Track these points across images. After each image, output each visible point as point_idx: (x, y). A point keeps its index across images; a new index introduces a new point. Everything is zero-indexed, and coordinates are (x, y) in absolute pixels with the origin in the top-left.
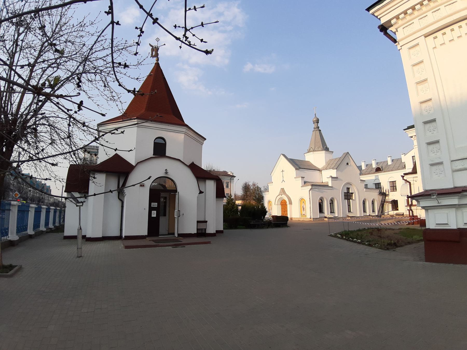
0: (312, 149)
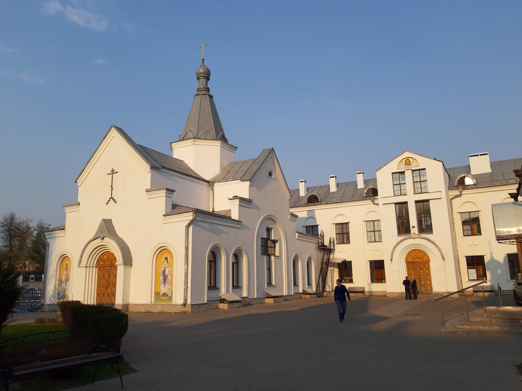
0: (191, 135)
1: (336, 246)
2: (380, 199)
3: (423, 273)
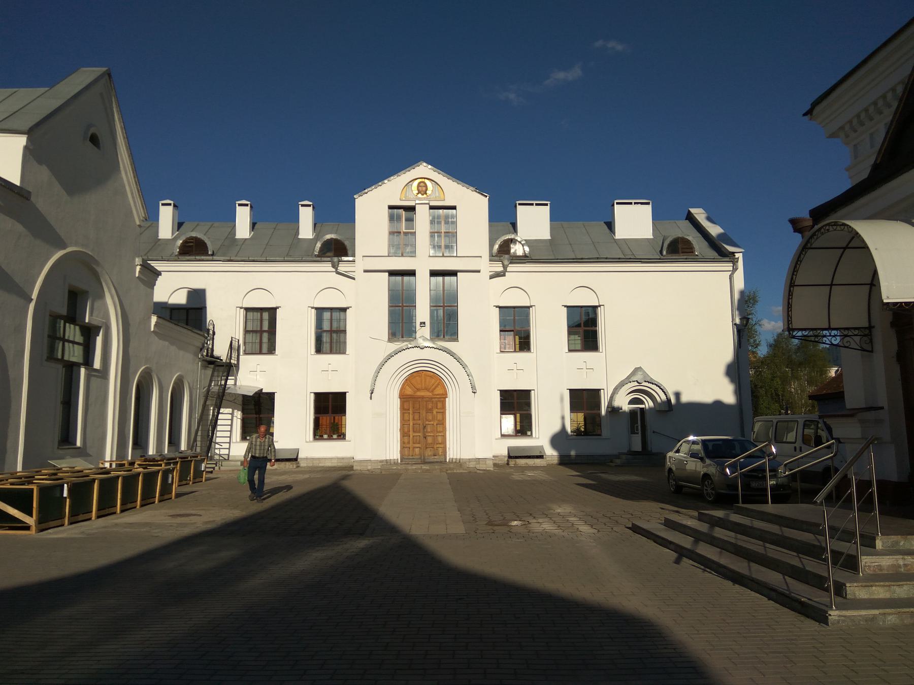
1: (242, 358)
2: (357, 264)
3: (433, 419)
